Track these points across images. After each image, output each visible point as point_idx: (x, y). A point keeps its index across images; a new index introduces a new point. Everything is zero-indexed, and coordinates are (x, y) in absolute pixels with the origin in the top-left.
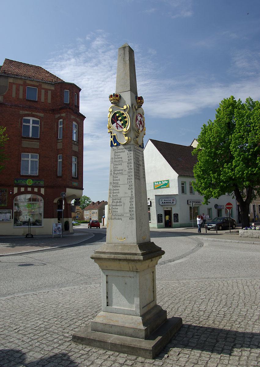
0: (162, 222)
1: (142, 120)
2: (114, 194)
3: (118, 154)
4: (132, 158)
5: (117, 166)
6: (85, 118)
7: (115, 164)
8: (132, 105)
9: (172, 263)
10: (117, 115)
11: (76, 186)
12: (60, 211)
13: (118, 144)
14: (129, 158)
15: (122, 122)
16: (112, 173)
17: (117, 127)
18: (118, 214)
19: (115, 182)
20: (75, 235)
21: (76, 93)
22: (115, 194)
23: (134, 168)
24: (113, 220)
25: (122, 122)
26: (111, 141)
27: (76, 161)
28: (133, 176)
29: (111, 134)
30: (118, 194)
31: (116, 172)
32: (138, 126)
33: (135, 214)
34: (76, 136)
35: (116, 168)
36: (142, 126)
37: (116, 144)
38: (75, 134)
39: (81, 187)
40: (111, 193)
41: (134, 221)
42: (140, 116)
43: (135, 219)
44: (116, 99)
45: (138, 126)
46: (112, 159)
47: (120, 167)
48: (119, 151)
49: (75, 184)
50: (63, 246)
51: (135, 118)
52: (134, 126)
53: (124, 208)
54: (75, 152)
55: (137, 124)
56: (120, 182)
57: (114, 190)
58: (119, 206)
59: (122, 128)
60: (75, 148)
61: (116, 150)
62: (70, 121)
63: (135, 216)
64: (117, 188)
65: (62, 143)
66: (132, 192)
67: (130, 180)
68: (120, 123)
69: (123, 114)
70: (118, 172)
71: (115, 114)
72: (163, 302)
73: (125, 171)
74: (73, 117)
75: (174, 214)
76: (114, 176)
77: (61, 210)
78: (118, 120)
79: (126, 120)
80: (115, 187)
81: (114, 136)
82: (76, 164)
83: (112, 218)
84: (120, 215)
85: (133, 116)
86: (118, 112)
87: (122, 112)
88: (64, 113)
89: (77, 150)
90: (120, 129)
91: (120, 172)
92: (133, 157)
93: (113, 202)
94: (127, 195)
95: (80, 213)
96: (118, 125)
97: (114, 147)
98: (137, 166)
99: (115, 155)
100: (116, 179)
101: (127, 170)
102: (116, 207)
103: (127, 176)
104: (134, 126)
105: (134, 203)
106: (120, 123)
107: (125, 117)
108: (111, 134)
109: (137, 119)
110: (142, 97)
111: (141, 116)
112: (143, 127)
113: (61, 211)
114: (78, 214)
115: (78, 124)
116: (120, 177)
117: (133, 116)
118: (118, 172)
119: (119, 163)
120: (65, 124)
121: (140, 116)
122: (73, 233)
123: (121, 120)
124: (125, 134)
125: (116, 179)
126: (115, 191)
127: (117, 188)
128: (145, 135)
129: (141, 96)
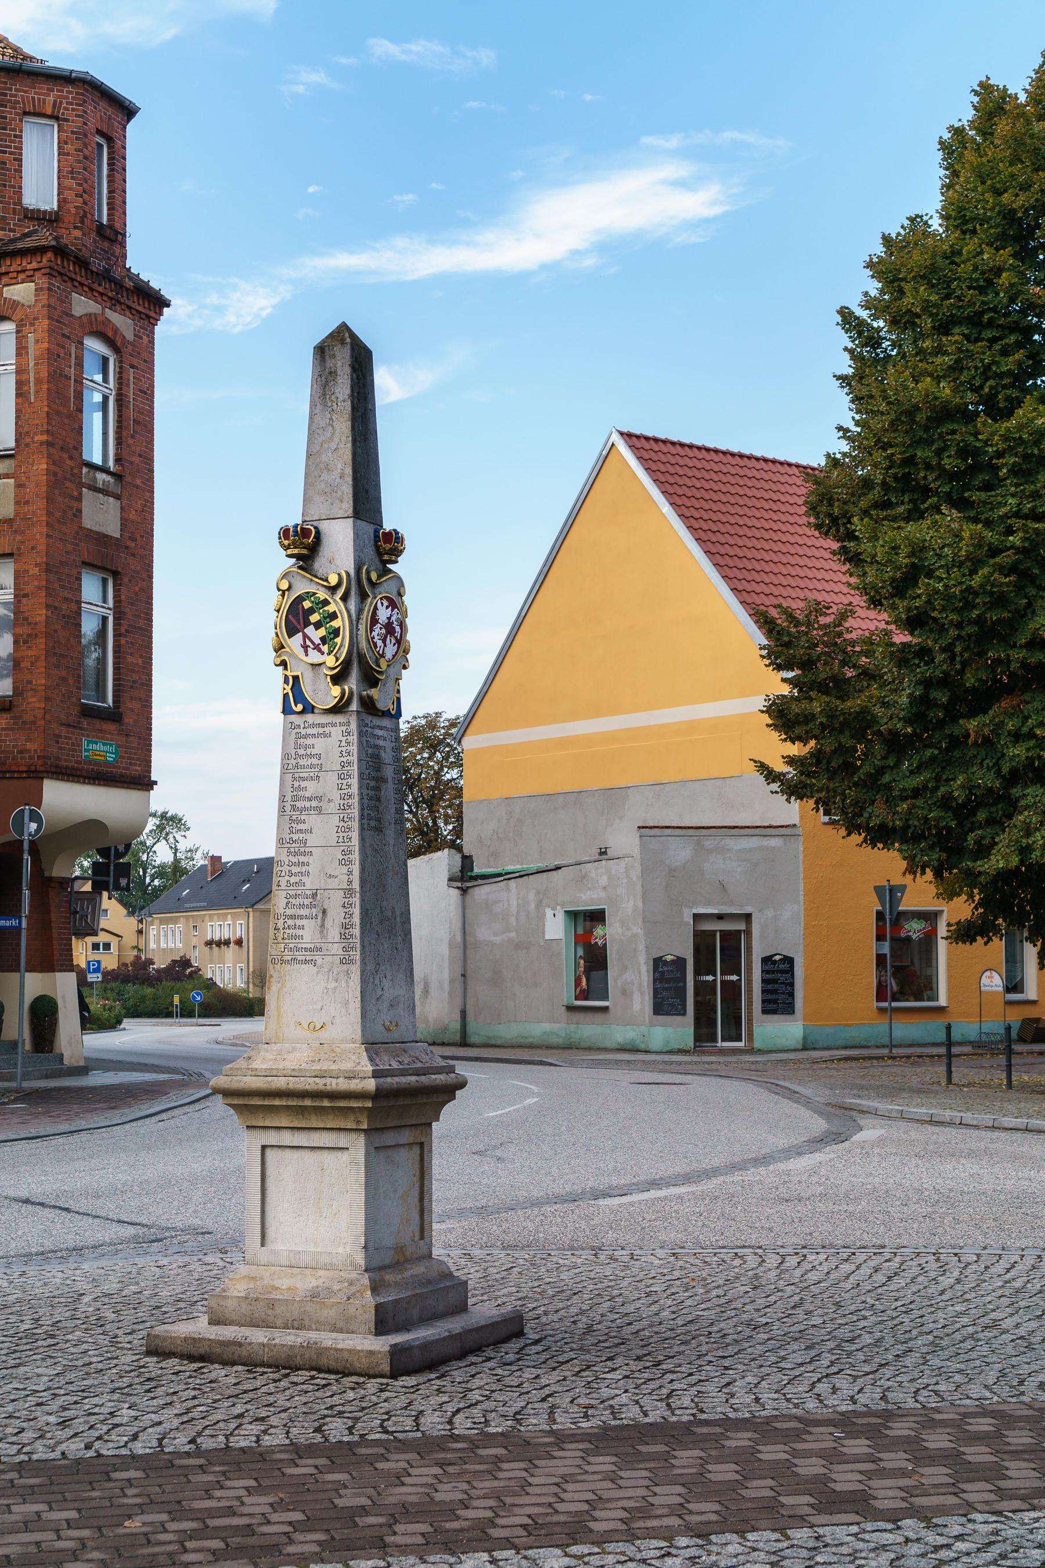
0: (684, 1014)
1: (393, 619)
2: (293, 880)
3: (309, 741)
4: (354, 758)
5: (303, 784)
6: (168, 305)
7: (297, 775)
8: (358, 570)
9: (609, 1201)
10: (307, 604)
11: (108, 764)
12: (8, 924)
13: (308, 709)
14: (342, 759)
15: (322, 632)
16: (288, 808)
17: (305, 647)
18: (304, 946)
19: (295, 837)
20: (98, 1079)
21: (99, 140)
22: (297, 879)
23: (361, 794)
24: (287, 967)
25: (322, 632)
26: (286, 696)
27: (105, 600)
28: (357, 820)
29: (286, 668)
30: (304, 879)
31: (298, 804)
32: (380, 643)
33: (358, 945)
34: (105, 433)
35: (300, 788)
36: (393, 641)
37: (300, 708)
38: (98, 417)
39: (137, 770)
40: (283, 874)
41: (356, 970)
42: (387, 607)
43: (358, 962)
44: (304, 544)
45: (380, 643)
46: (286, 756)
47: (311, 788)
48: (310, 731)
49: (101, 750)
50: (34, 1132)
51: (366, 615)
52: (363, 645)
53: (323, 926)
54: (102, 539)
55: (373, 638)
56: (312, 840)
57: (294, 864)
58: (306, 917)
59: (323, 653)
60: (101, 515)
61: (302, 726)
62: (66, 332)
63: (359, 953)
64: (302, 859)
65: (12, 481)
66: (350, 873)
67: (346, 834)
68: (316, 635)
69: (326, 603)
70: (308, 804)
71: (300, 599)
72: (449, 1242)
73: (330, 801)
74: (82, 305)
75: (766, 960)
76: (294, 817)
77: (14, 923)
78: (307, 623)
79: (335, 624)
80: (296, 854)
81: (296, 678)
82: (105, 619)
83: (286, 958)
84: (311, 950)
85: (360, 611)
86: (309, 595)
87: (322, 595)
88: (21, 276)
89: (113, 529)
90: (314, 657)
91: (314, 804)
92: (356, 755)
93: (287, 903)
94: (333, 884)
95: (114, 942)
96: (308, 643)
97: (293, 718)
98: (373, 784)
99: (298, 746)
100: (302, 826)
101: (337, 801)
102: (299, 922)
103: (335, 820)
104: (363, 645)
105: (357, 911)
106: (316, 635)
107: (333, 616)
108: (286, 668)
109: (374, 621)
110: (397, 533)
111: (392, 604)
112: (399, 642)
113: (12, 927)
114: (96, 946)
115: (116, 350)
116: (312, 820)
117: (360, 611)
118: (308, 804)
119: (312, 774)
120: (31, 357)
121: (387, 607)
122: (83, 1071)
123: (318, 625)
124: (331, 676)
125: (302, 826)
126: (295, 869)
127: (302, 859)
128: (405, 667)
129: (395, 530)
